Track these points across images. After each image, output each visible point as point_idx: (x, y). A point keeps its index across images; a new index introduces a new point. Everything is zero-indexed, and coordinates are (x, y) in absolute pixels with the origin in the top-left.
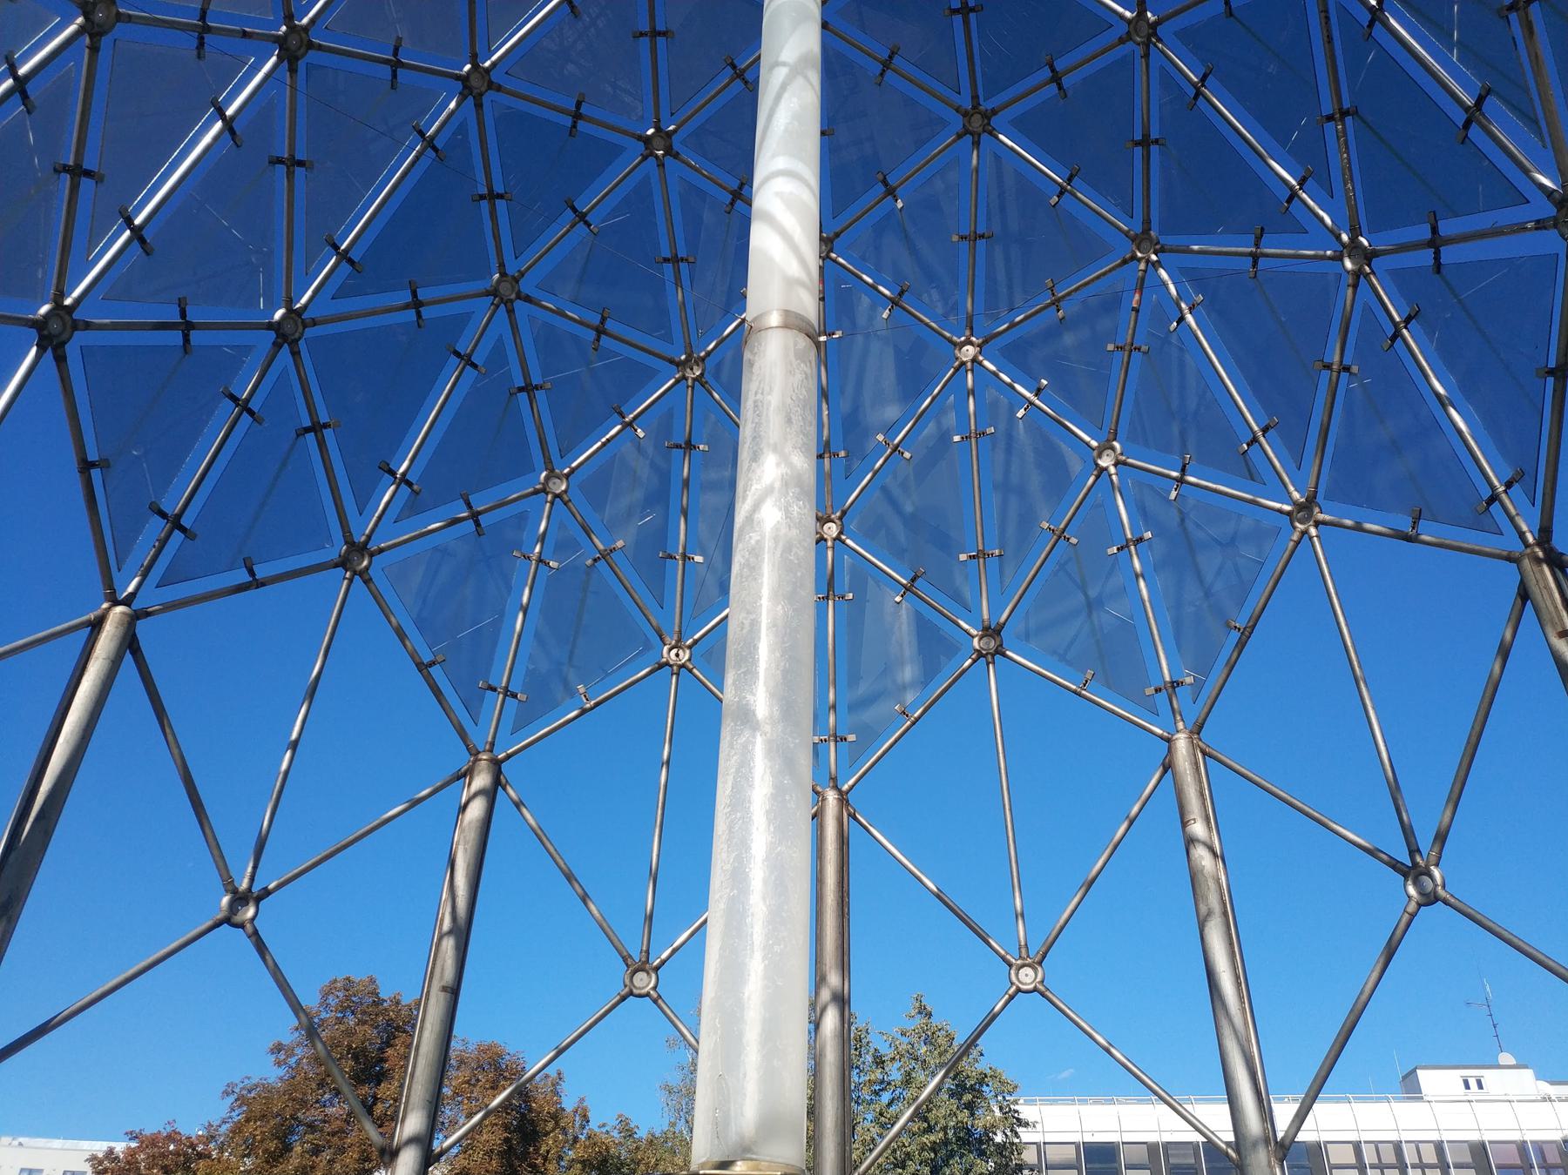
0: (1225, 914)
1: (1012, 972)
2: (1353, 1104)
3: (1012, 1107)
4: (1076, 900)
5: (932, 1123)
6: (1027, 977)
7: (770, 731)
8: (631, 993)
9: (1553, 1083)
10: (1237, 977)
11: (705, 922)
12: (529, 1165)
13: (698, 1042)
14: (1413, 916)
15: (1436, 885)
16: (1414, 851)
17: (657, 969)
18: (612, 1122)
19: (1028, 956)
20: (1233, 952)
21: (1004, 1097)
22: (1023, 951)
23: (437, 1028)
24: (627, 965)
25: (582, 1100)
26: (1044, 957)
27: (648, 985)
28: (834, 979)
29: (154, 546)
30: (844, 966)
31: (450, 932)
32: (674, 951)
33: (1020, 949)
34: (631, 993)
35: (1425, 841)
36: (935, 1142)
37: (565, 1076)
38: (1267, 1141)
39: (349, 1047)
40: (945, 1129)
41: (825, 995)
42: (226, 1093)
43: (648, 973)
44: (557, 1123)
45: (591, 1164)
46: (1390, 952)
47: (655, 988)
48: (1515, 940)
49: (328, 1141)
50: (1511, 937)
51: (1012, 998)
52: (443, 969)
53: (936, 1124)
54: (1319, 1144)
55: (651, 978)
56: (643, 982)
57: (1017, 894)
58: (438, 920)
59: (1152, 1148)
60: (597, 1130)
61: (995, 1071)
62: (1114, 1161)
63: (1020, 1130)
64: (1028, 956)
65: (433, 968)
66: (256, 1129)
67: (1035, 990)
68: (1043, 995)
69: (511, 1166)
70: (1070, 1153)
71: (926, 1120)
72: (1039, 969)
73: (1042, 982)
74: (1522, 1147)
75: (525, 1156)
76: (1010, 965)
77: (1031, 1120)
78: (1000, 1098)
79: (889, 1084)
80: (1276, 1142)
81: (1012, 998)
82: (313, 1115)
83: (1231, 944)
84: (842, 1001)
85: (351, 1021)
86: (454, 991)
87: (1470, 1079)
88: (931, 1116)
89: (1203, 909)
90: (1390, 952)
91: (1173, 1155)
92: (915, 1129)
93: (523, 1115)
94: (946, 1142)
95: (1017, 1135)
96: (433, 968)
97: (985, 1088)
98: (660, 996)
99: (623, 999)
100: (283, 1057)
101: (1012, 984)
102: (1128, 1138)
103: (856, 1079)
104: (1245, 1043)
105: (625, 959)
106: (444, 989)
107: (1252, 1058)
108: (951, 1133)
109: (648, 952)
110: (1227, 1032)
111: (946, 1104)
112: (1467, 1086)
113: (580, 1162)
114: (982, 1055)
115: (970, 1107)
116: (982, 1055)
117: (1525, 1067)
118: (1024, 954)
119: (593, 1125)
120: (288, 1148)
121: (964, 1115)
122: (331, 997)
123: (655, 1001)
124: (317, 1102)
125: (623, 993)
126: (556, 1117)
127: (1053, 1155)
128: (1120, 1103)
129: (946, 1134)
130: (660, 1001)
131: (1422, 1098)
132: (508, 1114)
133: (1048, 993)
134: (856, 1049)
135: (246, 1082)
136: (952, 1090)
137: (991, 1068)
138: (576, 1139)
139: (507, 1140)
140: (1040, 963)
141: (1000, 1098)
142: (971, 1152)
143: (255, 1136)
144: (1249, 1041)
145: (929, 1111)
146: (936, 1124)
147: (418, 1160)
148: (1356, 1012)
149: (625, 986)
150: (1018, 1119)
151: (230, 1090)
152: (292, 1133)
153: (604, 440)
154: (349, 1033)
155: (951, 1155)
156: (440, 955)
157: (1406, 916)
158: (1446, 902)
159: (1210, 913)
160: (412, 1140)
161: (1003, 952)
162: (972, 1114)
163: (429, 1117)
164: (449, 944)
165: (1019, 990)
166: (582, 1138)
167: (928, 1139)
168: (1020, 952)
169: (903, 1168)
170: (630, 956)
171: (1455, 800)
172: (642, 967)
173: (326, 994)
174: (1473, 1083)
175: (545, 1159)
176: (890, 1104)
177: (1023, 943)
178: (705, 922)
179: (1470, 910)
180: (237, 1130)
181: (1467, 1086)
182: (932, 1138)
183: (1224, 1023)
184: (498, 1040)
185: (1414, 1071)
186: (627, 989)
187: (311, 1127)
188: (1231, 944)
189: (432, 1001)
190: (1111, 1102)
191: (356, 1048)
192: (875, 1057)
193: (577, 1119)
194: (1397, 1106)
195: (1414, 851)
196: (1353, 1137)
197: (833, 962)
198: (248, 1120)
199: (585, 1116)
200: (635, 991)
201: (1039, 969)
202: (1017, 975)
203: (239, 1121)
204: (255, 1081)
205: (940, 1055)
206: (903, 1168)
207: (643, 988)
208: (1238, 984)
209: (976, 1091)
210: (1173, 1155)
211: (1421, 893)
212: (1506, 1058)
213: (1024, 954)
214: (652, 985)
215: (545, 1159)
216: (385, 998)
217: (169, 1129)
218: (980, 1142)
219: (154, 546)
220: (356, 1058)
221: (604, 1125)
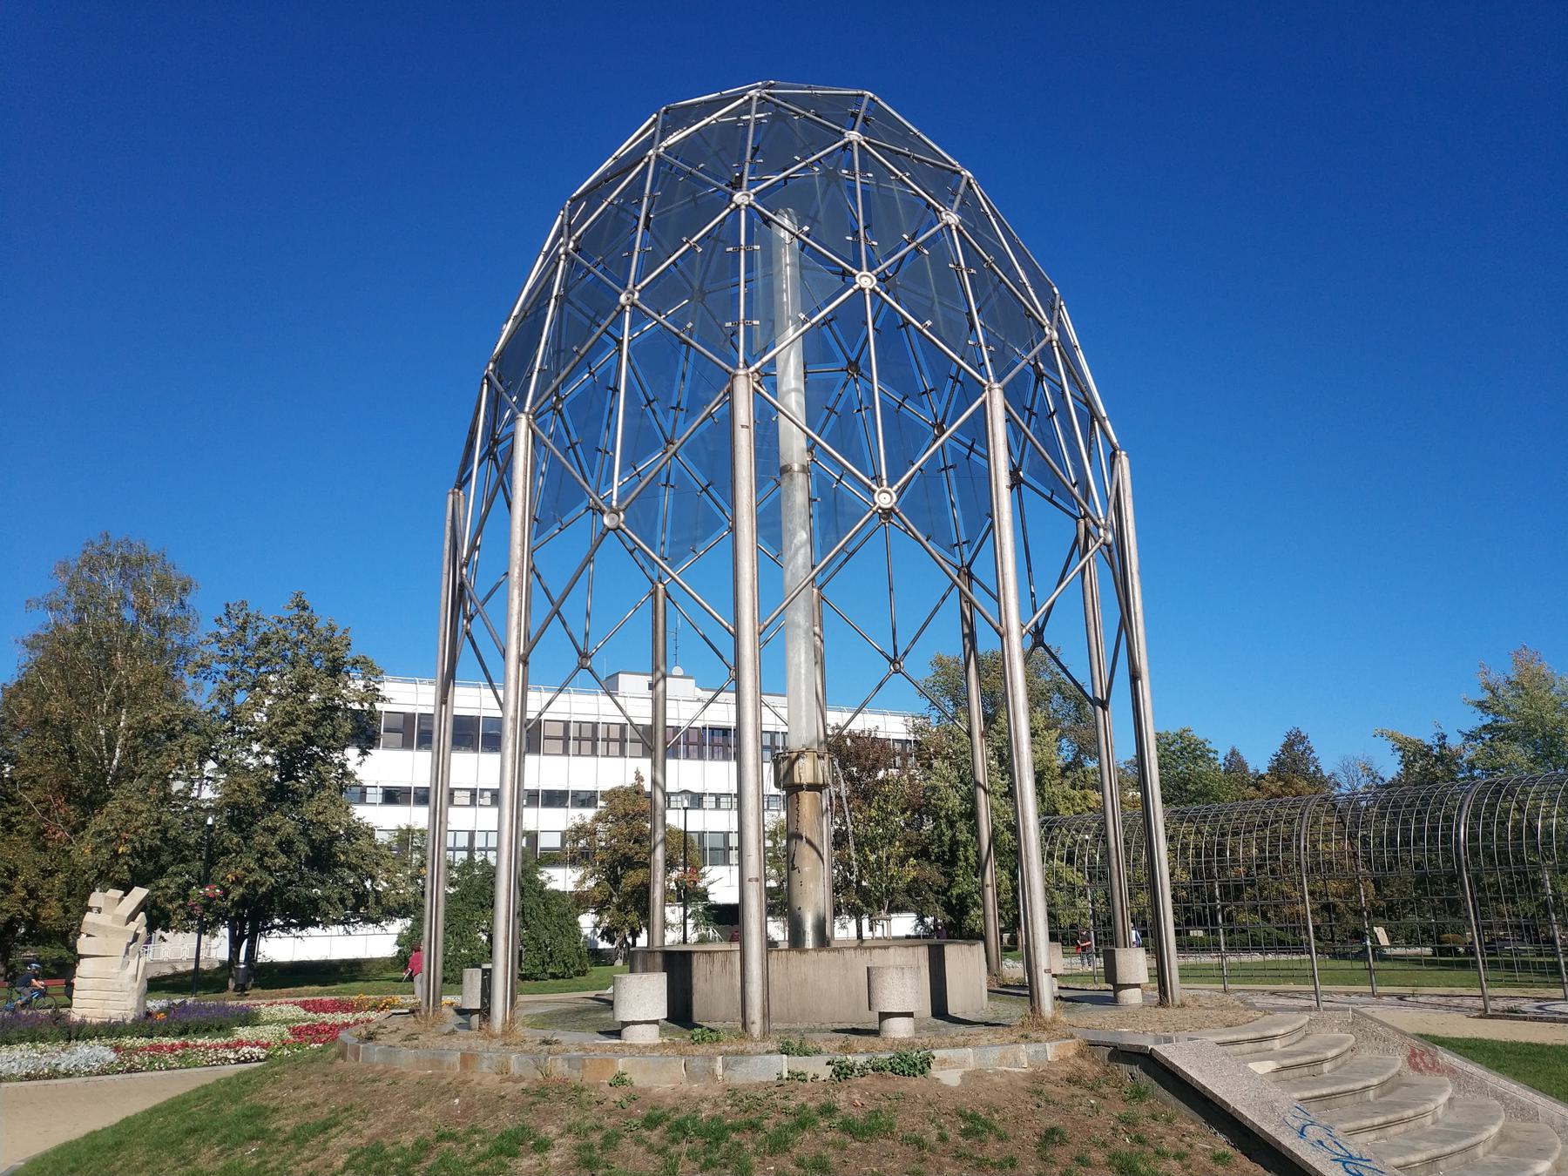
2: (482, 690)
7: (1077, 900)
9: (702, 690)
16: (896, 655)
29: (1215, 1133)
35: (900, 653)
46: (880, 686)
77: (388, 696)
90: (880, 686)
117: (691, 678)
153: (876, 98)
171: (914, 641)
195: (896, 655)
196: (565, 718)
219: (1215, 1133)
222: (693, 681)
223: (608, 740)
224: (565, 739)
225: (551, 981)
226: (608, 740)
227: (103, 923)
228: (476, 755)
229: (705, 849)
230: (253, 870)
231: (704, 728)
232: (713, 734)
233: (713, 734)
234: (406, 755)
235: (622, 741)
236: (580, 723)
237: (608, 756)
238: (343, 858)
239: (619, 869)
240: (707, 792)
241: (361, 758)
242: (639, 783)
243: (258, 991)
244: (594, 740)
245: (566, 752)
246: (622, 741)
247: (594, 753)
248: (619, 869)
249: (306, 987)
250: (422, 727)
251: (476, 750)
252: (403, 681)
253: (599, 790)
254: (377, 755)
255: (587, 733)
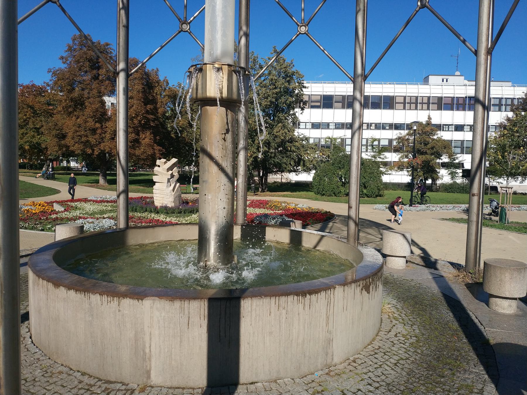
0: (364, 10)
1: (299, 28)
3: (302, 82)
4: (321, 5)
5: (276, 86)
6: (303, 29)
8: (182, 31)
9: (468, 81)
10: (364, 30)
11: (204, 8)
12: (152, 96)
13: (204, 47)
14: (417, 12)
15: (426, 2)
17: (189, 23)
18: (176, 84)
19: (304, 23)
20: (364, 22)
21: (299, 79)
22: (303, 21)
23: (124, 38)
24: (180, 21)
25: (166, 77)
26: (309, 23)
27: (187, 28)
28: (244, 28)
30: (248, 25)
31: (123, 8)
32: (194, 18)
33: (302, 20)
34: (182, 31)
36: (277, 92)
37: (159, 69)
38: (362, 75)
39: (86, 58)
40: (280, 88)
41: (242, 33)
42: (49, 72)
43: (187, 24)
44: (158, 84)
45: (171, 96)
47: (189, 29)
48: (439, 16)
49: (86, 87)
50: (437, 14)
51: (298, 35)
52: (122, 20)
53: (278, 87)
54: (394, 96)
55: (188, 26)
56: (186, 27)
57: (303, 3)
58: (118, 4)
59: (344, 97)
60: (171, 87)
61: (297, 71)
62: (332, 100)
63: (304, 89)
64: (304, 23)
65: (119, 20)
66: (62, 83)
67: (305, 33)
68: (307, 35)
69: (146, 96)
70: (319, 98)
71: (275, 85)
72: (307, 27)
73: (307, 31)
74: (453, 98)
75: (150, 93)
76: (298, 25)
78: (298, 79)
79: (264, 74)
80: (364, 76)
81: (298, 35)
82: (79, 79)
83: (364, 20)
84: (247, 35)
85: (85, 49)
86: (127, 27)
87: (444, 79)
88: (276, 84)
89: (358, 9)
91: (349, 99)
92: (271, 88)
93: (148, 81)
94: (280, 92)
95: (302, 91)
96: (119, 20)
97: (294, 76)
98: (191, 32)
99: (180, 32)
100: (65, 61)
101: (298, 31)
102: (337, 94)
103: (254, 73)
104: (362, 49)
105: (179, 20)
106: (124, 26)
107: (363, 53)
108: (282, 90)
109: (186, 18)
110: (357, 46)
111: (281, 81)
112: (443, 81)
113: (168, 96)
114: (294, 66)
115: (289, 82)
116: (294, 66)
117: (463, 76)
118: (303, 22)
119: (170, 85)
120: (74, 89)
121: (286, 84)
122: (76, 41)
123: (190, 33)
124: (80, 75)
125: (179, 30)
126: (158, 82)
127: (313, 98)
128: (336, 83)
129: (281, 89)
130: (191, 33)
131: (428, 84)
132: (142, 80)
133: (308, 34)
134: (253, 63)
135: (54, 69)
136: (283, 77)
137: (296, 70)
138: (165, 89)
139: (143, 88)
140: (307, 25)
141: (298, 79)
142: (288, 95)
143: (62, 85)
144: (363, 49)
145: (276, 82)
146: (278, 87)
147: (125, 75)
148: (394, 40)
149: (180, 28)
150: (303, 86)
151: (50, 70)
152: (74, 84)
154: (85, 53)
155: (282, 95)
156: (121, 15)
157: (415, 12)
158: (427, 7)
159: (359, 10)
160: (122, 70)
161: (296, 21)
162: (289, 84)
163: (126, 64)
164: (123, 12)
165: (300, 33)
166: (167, 89)
167: (274, 91)
168: (302, 22)
169: (267, 99)
170: (181, 19)
172: (185, 22)
173: (74, 40)
174: (445, 80)
175: (156, 94)
176: (264, 81)
177: (303, 19)
178: (204, 8)
179: (433, 10)
180: (55, 83)
181: (443, 81)
182: (276, 91)
183: (357, 43)
184: (136, 57)
185: (428, 76)
186: (180, 29)
187: (80, 82)
188: (364, 20)
189: (121, 30)
190: (333, 83)
191: (89, 58)
192: (260, 66)
193: (165, 83)
194: (420, 86)
196: (404, 95)
197: (244, 23)
198: (58, 80)
199: (167, 82)
200: (183, 30)
201: (307, 27)
202: (300, 29)
203: (56, 80)
204: (57, 68)
205: (281, 65)
206: (267, 99)
207: (186, 29)
208: (364, 32)
209: (291, 78)
210: (349, 99)
211: (421, 4)
212: (458, 73)
213: (303, 22)
214: (188, 28)
215: (156, 94)
216: (95, 42)
217: (32, 83)
218: (291, 92)
220: (89, 61)
221: (174, 85)
222: (463, 77)
223: (422, 103)
224: (404, 103)
225: (366, 198)
226: (422, 103)
227: (160, 171)
228: (381, 110)
229: (464, 147)
230: (256, 153)
231: (466, 97)
232: (470, 100)
233: (470, 100)
234: (343, 111)
235: (428, 103)
236: (423, 97)
237: (422, 109)
238: (289, 148)
239: (417, 154)
240: (466, 124)
241: (302, 111)
242: (429, 121)
243: (268, 193)
244: (416, 103)
245: (404, 108)
246: (428, 103)
247: (416, 109)
248: (417, 154)
249: (278, 193)
250: (349, 100)
251: (369, 109)
252: (342, 83)
253: (442, 124)
254: (307, 111)
255: (413, 100)
